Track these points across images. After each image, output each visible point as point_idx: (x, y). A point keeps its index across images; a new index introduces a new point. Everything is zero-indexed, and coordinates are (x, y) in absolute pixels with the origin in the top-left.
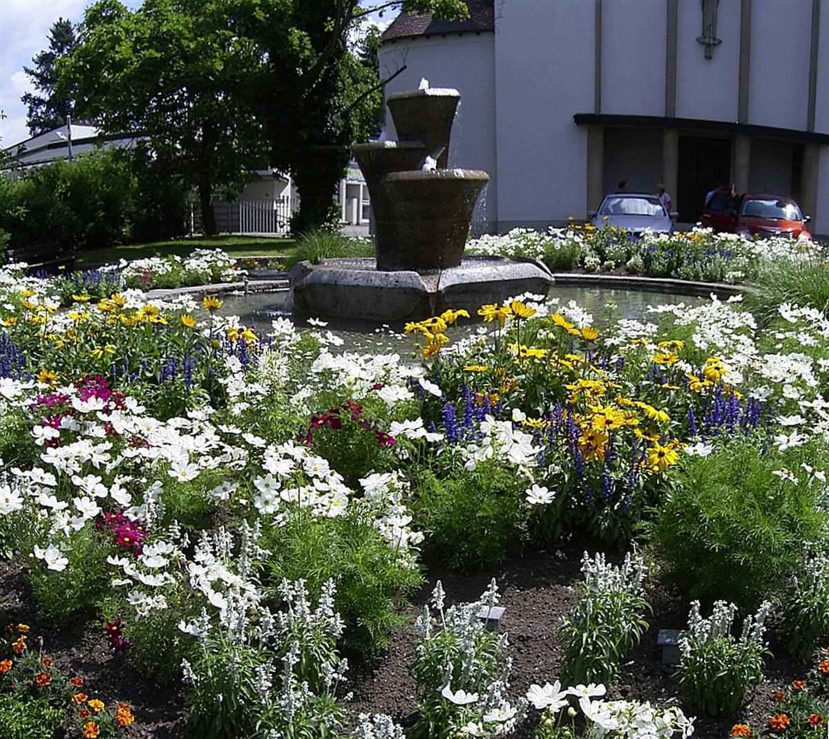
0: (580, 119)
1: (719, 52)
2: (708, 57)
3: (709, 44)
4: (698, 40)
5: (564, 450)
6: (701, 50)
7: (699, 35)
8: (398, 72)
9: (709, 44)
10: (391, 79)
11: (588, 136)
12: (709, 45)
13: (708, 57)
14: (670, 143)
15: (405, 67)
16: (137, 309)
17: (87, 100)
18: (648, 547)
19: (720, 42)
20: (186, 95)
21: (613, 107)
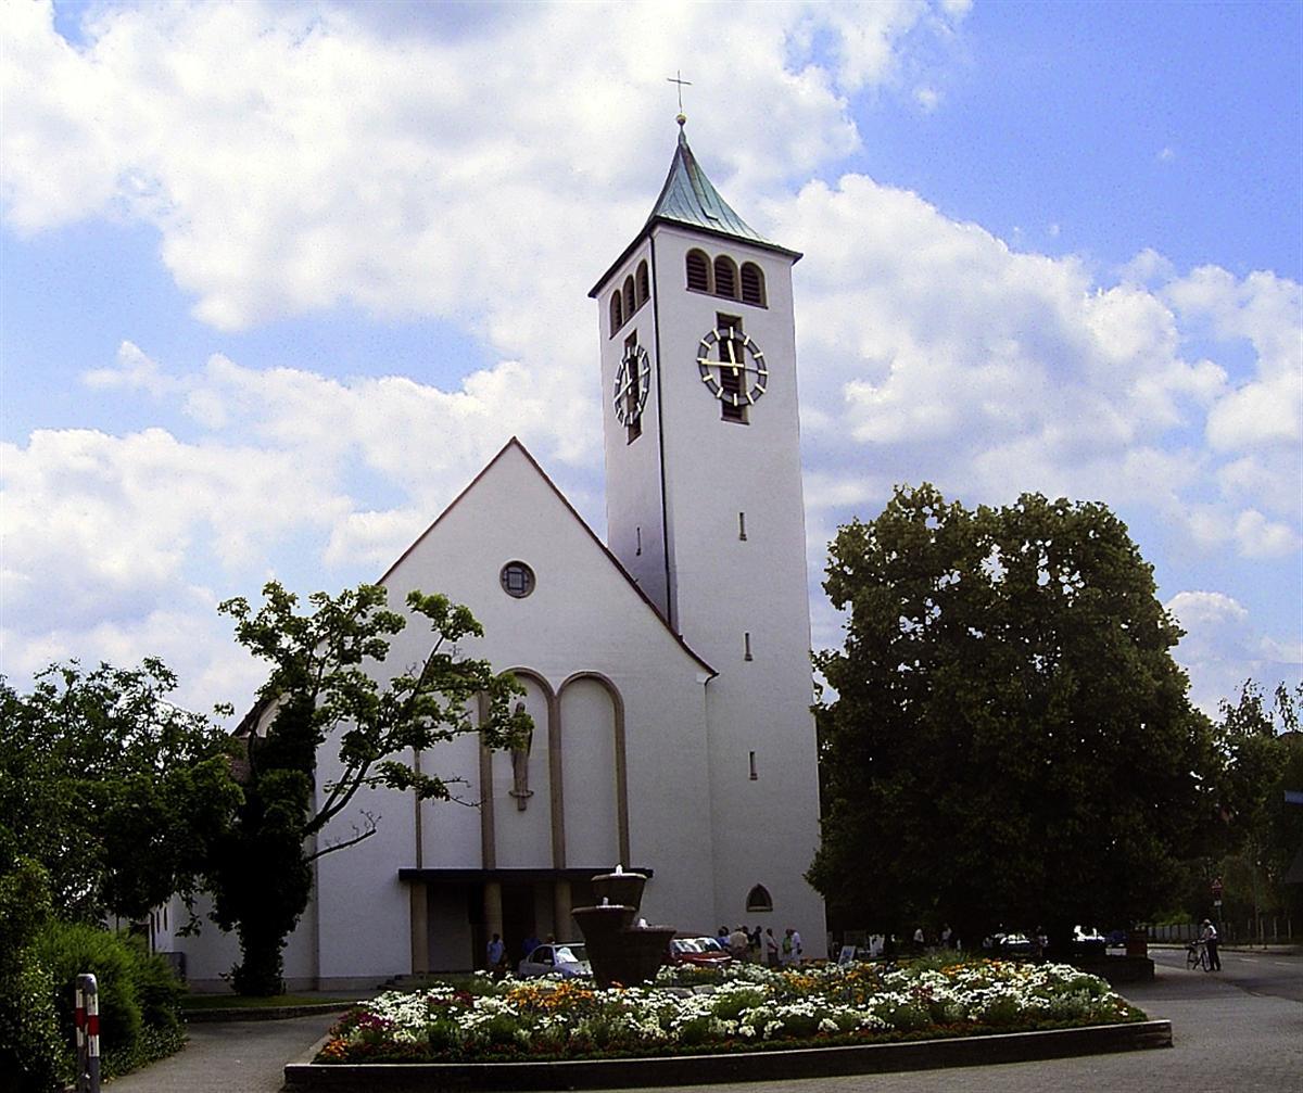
0: (405, 876)
1: (531, 803)
2: (522, 809)
3: (521, 797)
4: (510, 793)
5: (754, 973)
6: (514, 804)
7: (512, 788)
8: (367, 835)
9: (521, 797)
10: (358, 840)
11: (412, 892)
12: (523, 797)
13: (522, 809)
14: (494, 901)
15: (374, 831)
16: (838, 653)
17: (906, 600)
18: (1147, 927)
19: (532, 793)
20: (936, 589)
21: (430, 864)
